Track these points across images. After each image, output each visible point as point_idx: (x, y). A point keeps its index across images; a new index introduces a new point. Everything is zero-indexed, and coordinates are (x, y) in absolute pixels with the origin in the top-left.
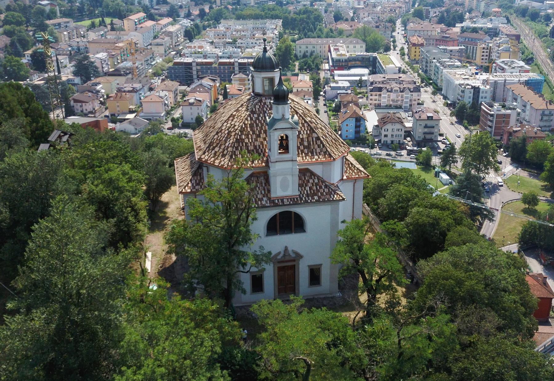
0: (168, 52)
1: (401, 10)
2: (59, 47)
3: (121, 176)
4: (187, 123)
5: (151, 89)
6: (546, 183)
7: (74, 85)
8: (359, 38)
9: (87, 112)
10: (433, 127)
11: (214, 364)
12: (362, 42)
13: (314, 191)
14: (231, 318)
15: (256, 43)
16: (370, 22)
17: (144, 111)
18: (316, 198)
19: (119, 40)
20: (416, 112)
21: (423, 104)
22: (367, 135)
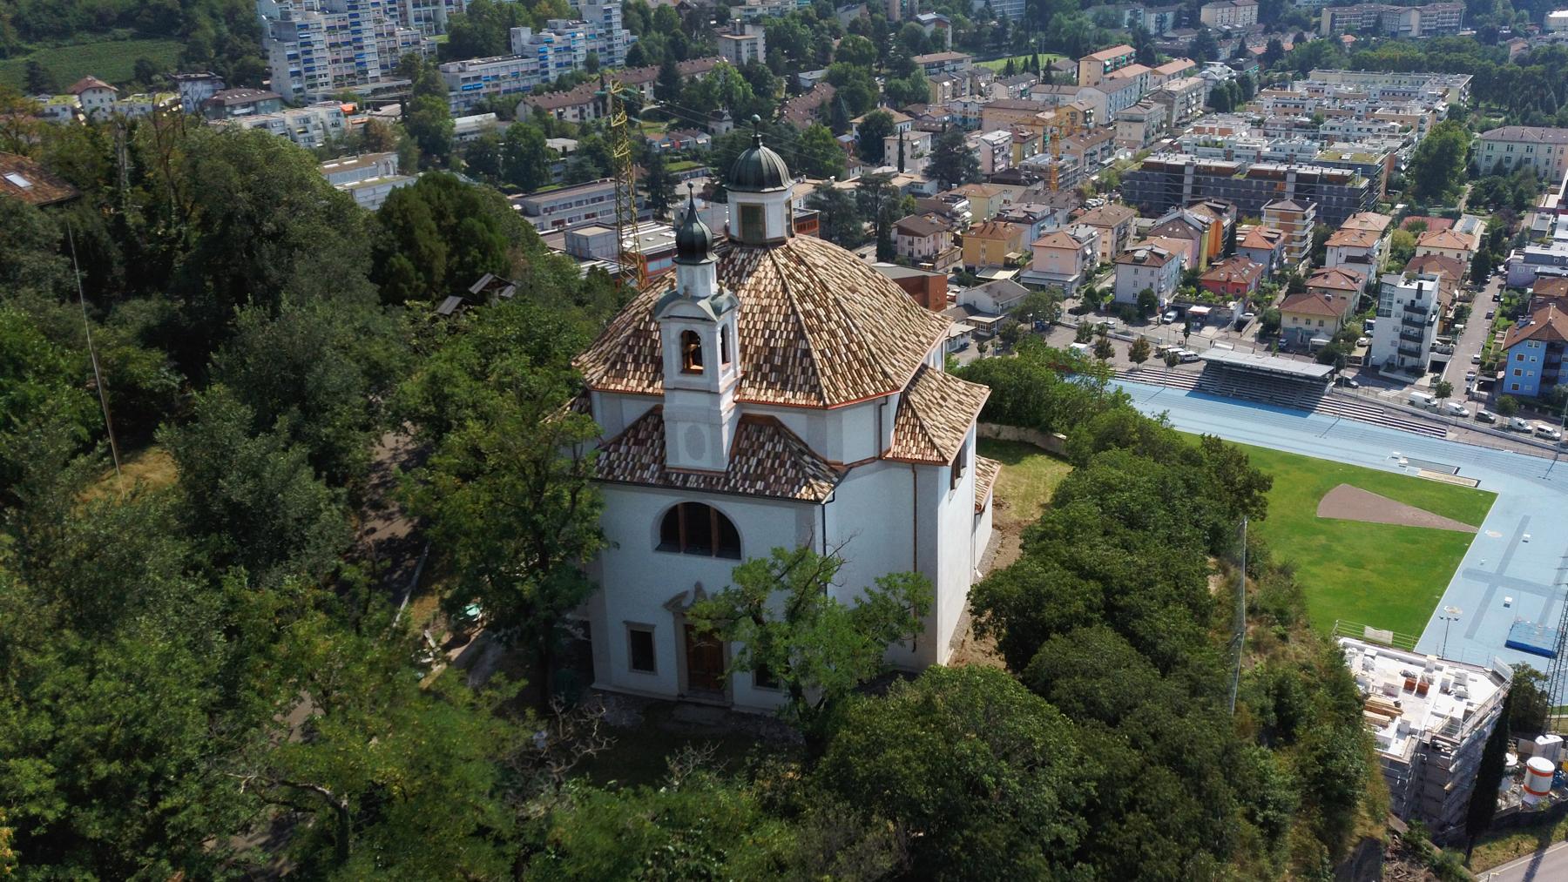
0: (1153, 139)
15: (1369, 130)
18: (760, 485)
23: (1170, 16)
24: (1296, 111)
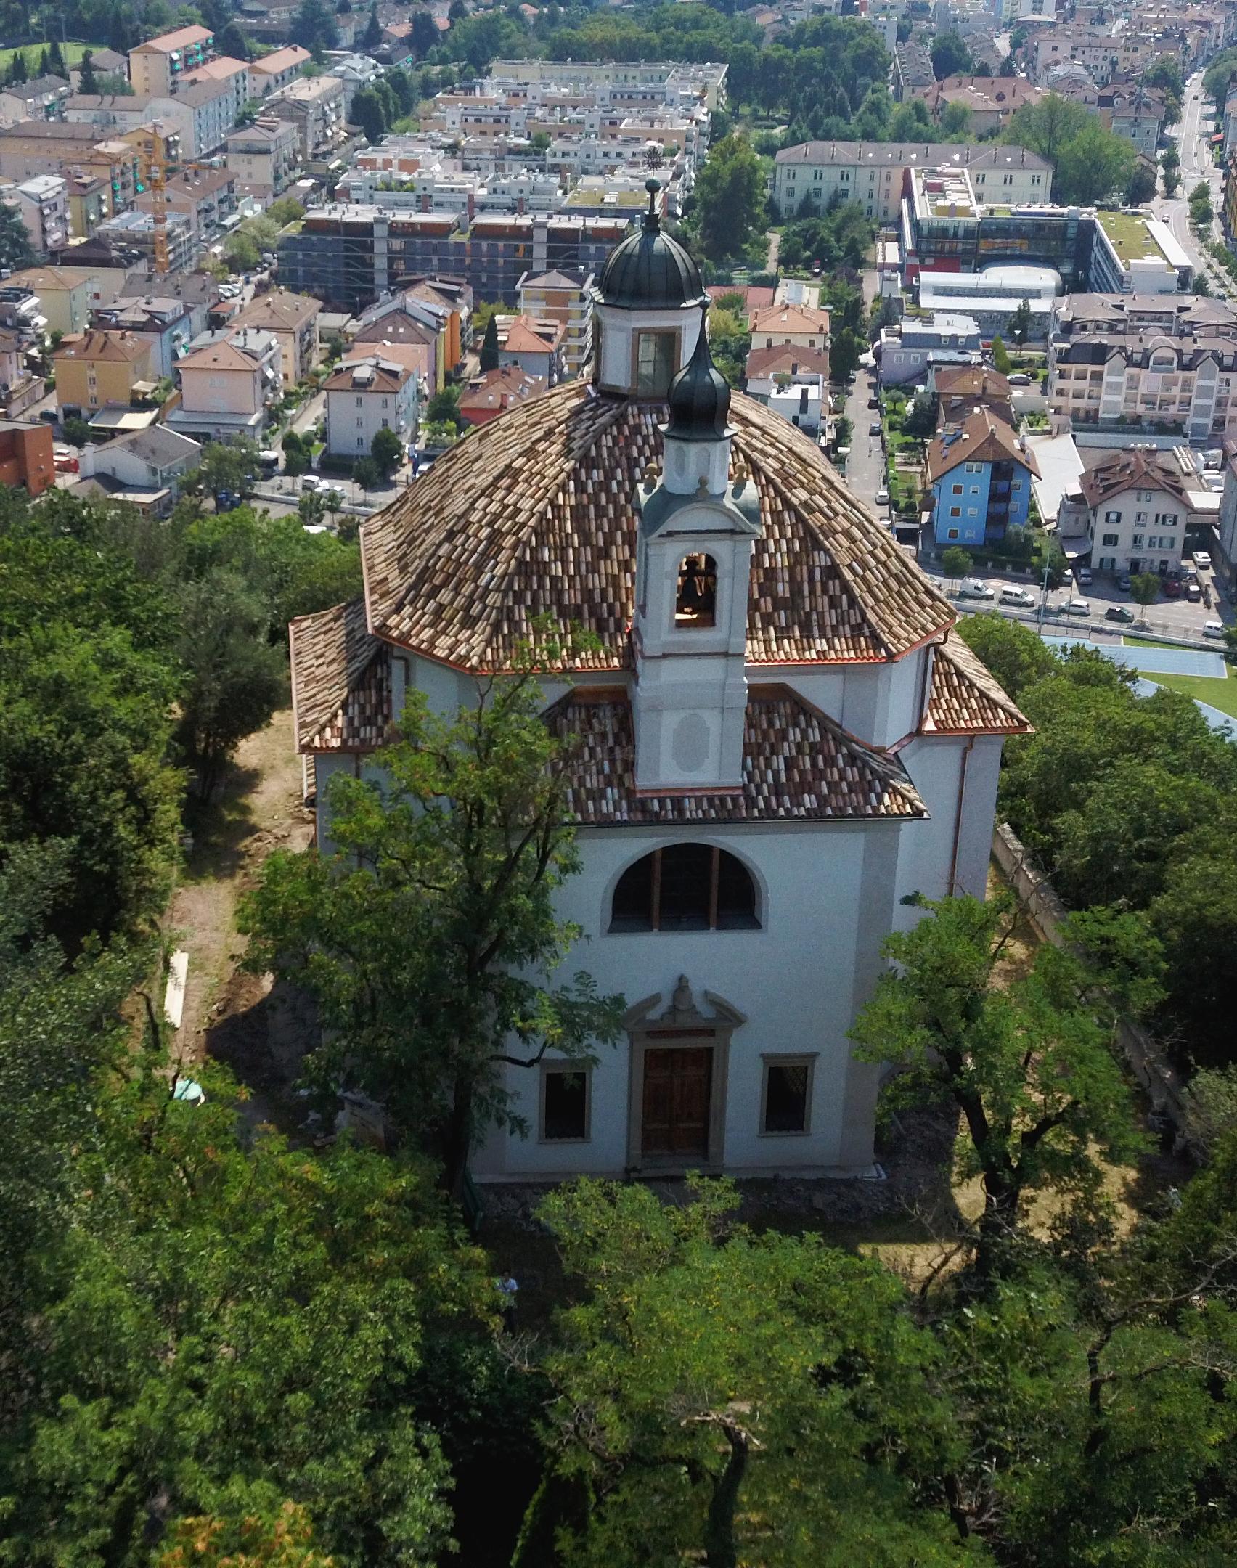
0: (285, 181)
1: (1206, 34)
3: (94, 669)
4: (340, 456)
5: (216, 322)
8: (1027, 146)
11: (389, 1407)
12: (1037, 161)
13: (802, 773)
14: (460, 1233)
15: (619, 155)
16: (1074, 82)
17: (188, 404)
18: (809, 801)
19: (108, 127)
22: (1034, 532)
24: (497, 127)
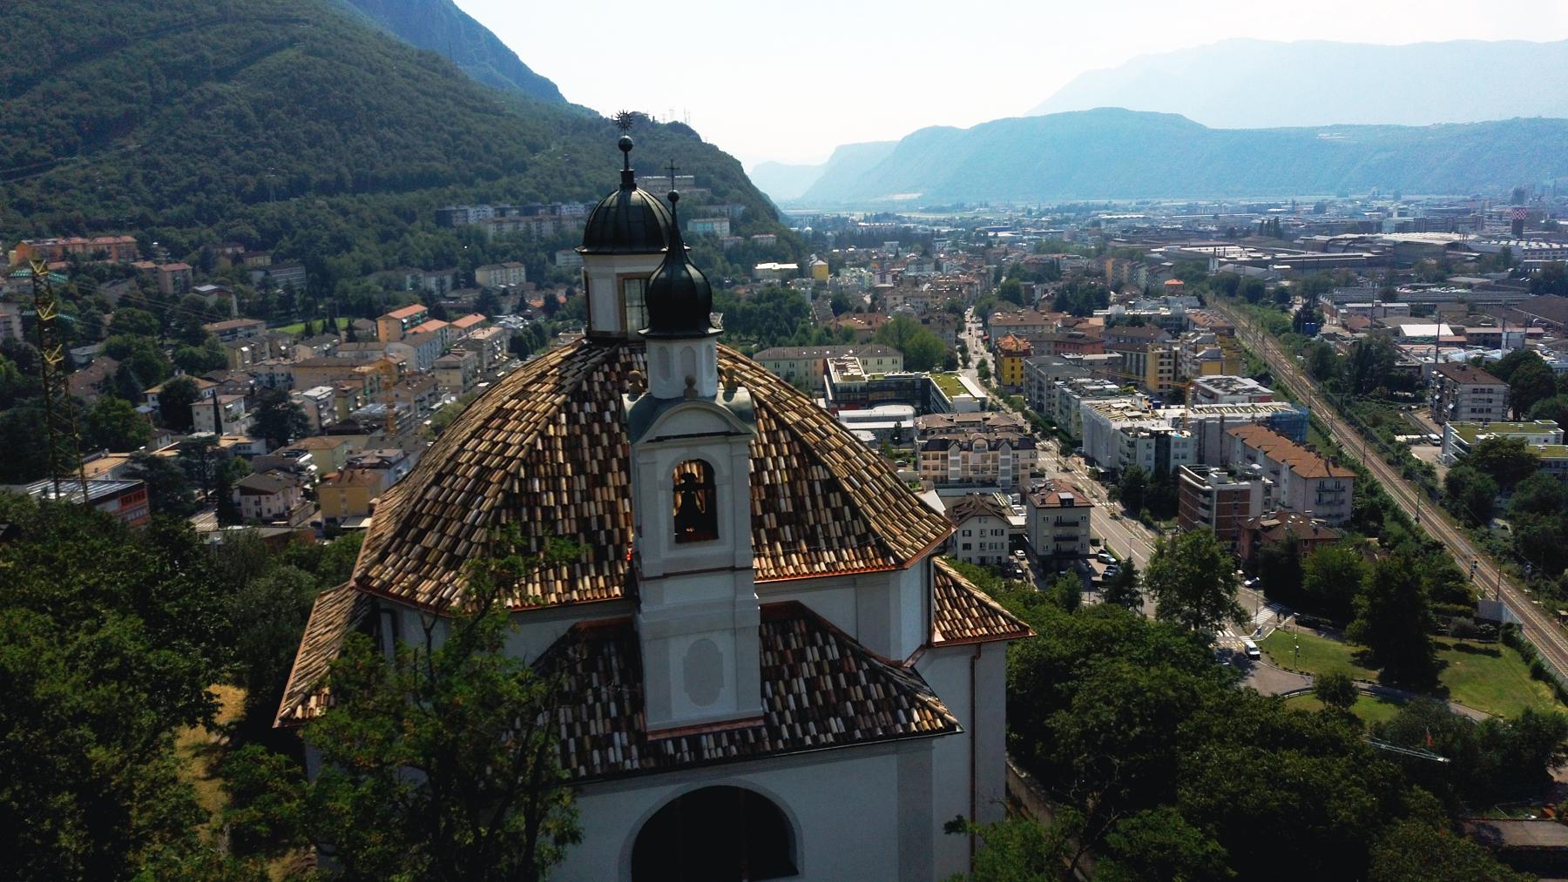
0: (471, 384)
2: (229, 377)
6: (1362, 648)
7: (249, 457)
8: (888, 344)
9: (270, 515)
10: (1076, 524)
12: (895, 351)
13: (825, 694)
18: (836, 725)
19: (363, 359)
20: (1033, 491)
21: (1044, 476)
23: (448, 279)
